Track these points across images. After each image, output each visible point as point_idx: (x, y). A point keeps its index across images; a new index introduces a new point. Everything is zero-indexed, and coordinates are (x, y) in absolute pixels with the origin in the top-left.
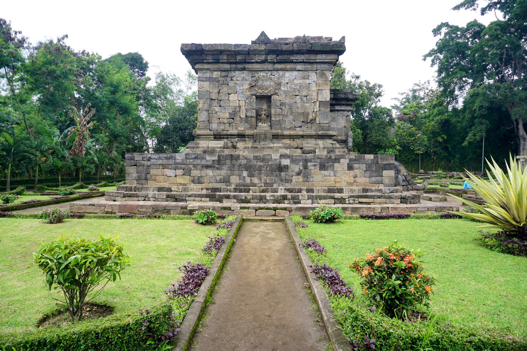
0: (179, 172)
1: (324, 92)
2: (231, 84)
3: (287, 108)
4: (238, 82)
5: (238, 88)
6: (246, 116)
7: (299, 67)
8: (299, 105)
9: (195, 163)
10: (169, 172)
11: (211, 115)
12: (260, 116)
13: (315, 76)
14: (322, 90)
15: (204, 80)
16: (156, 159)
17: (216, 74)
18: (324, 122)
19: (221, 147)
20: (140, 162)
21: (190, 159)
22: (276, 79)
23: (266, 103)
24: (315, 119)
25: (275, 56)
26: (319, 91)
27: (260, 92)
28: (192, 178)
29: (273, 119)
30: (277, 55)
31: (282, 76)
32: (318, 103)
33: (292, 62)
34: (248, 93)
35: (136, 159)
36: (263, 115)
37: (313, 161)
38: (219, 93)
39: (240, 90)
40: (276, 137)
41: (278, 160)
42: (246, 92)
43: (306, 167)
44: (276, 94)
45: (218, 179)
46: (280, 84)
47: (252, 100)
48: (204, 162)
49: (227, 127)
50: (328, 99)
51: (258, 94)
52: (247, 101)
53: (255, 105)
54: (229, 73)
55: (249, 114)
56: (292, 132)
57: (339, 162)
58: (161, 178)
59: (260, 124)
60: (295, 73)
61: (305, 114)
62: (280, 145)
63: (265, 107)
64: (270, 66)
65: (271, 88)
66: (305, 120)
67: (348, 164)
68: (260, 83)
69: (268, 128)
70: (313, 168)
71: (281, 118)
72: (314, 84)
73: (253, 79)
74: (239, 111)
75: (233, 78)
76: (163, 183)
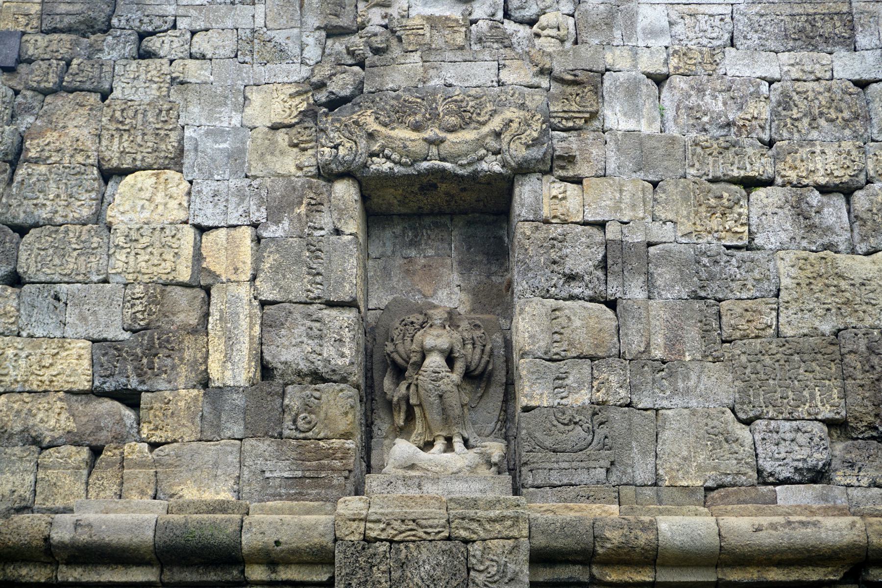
2: (136, 85)
3: (672, 289)
4: (194, 71)
5: (195, 119)
6: (266, 371)
8: (786, 270)
12: (399, 373)
22: (548, 44)
23: (466, 267)
29: (533, 392)
31: (609, 22)
36: (435, 361)
39: (216, 134)
42: (272, 149)
44: (555, 165)
46: (587, 82)
47: (326, 220)
51: (382, 165)
52: (271, 231)
53: (352, 265)
55: (289, 352)
59: (403, 448)
63: (451, 293)
68: (401, 74)
69: (491, 488)
71: (614, 384)
74: (202, 328)
75: (153, 43)
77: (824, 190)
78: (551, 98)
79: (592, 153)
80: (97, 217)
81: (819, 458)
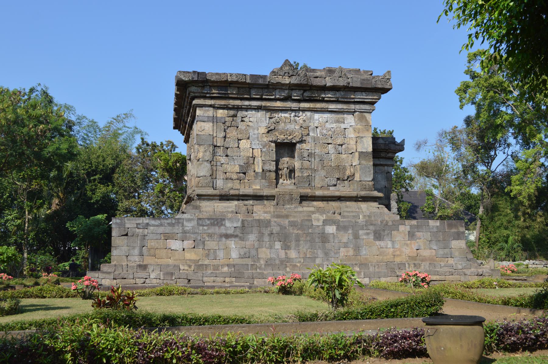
0: (188, 244)
1: (364, 140)
2: (242, 126)
3: (317, 160)
6: (263, 170)
7: (332, 106)
8: (333, 157)
9: (210, 231)
10: (175, 245)
11: (215, 168)
13: (353, 119)
14: (362, 137)
15: (206, 120)
16: (157, 226)
17: (221, 113)
18: (366, 179)
19: (232, 212)
20: (134, 230)
21: (203, 226)
24: (354, 175)
25: (302, 92)
26: (359, 139)
27: (281, 138)
28: (207, 252)
30: (305, 91)
32: (357, 154)
33: (323, 101)
34: (265, 139)
35: (127, 226)
37: (365, 228)
38: (225, 137)
39: (254, 134)
40: (304, 198)
41: (320, 227)
42: (263, 137)
43: (356, 237)
45: (242, 253)
48: (223, 230)
49: (236, 185)
50: (370, 149)
51: (279, 141)
54: (240, 112)
55: (267, 167)
56: (326, 193)
57: (398, 230)
58: (163, 253)
60: (326, 116)
61: (339, 168)
62: (312, 209)
64: (294, 105)
65: (297, 133)
66: (341, 176)
67: (409, 232)
68: (281, 126)
70: (365, 237)
72: (351, 129)
73: (272, 120)
76: (166, 260)
77: (339, 145)
78: (302, 131)
79: (308, 139)
80: (238, 147)
81: (335, 183)
